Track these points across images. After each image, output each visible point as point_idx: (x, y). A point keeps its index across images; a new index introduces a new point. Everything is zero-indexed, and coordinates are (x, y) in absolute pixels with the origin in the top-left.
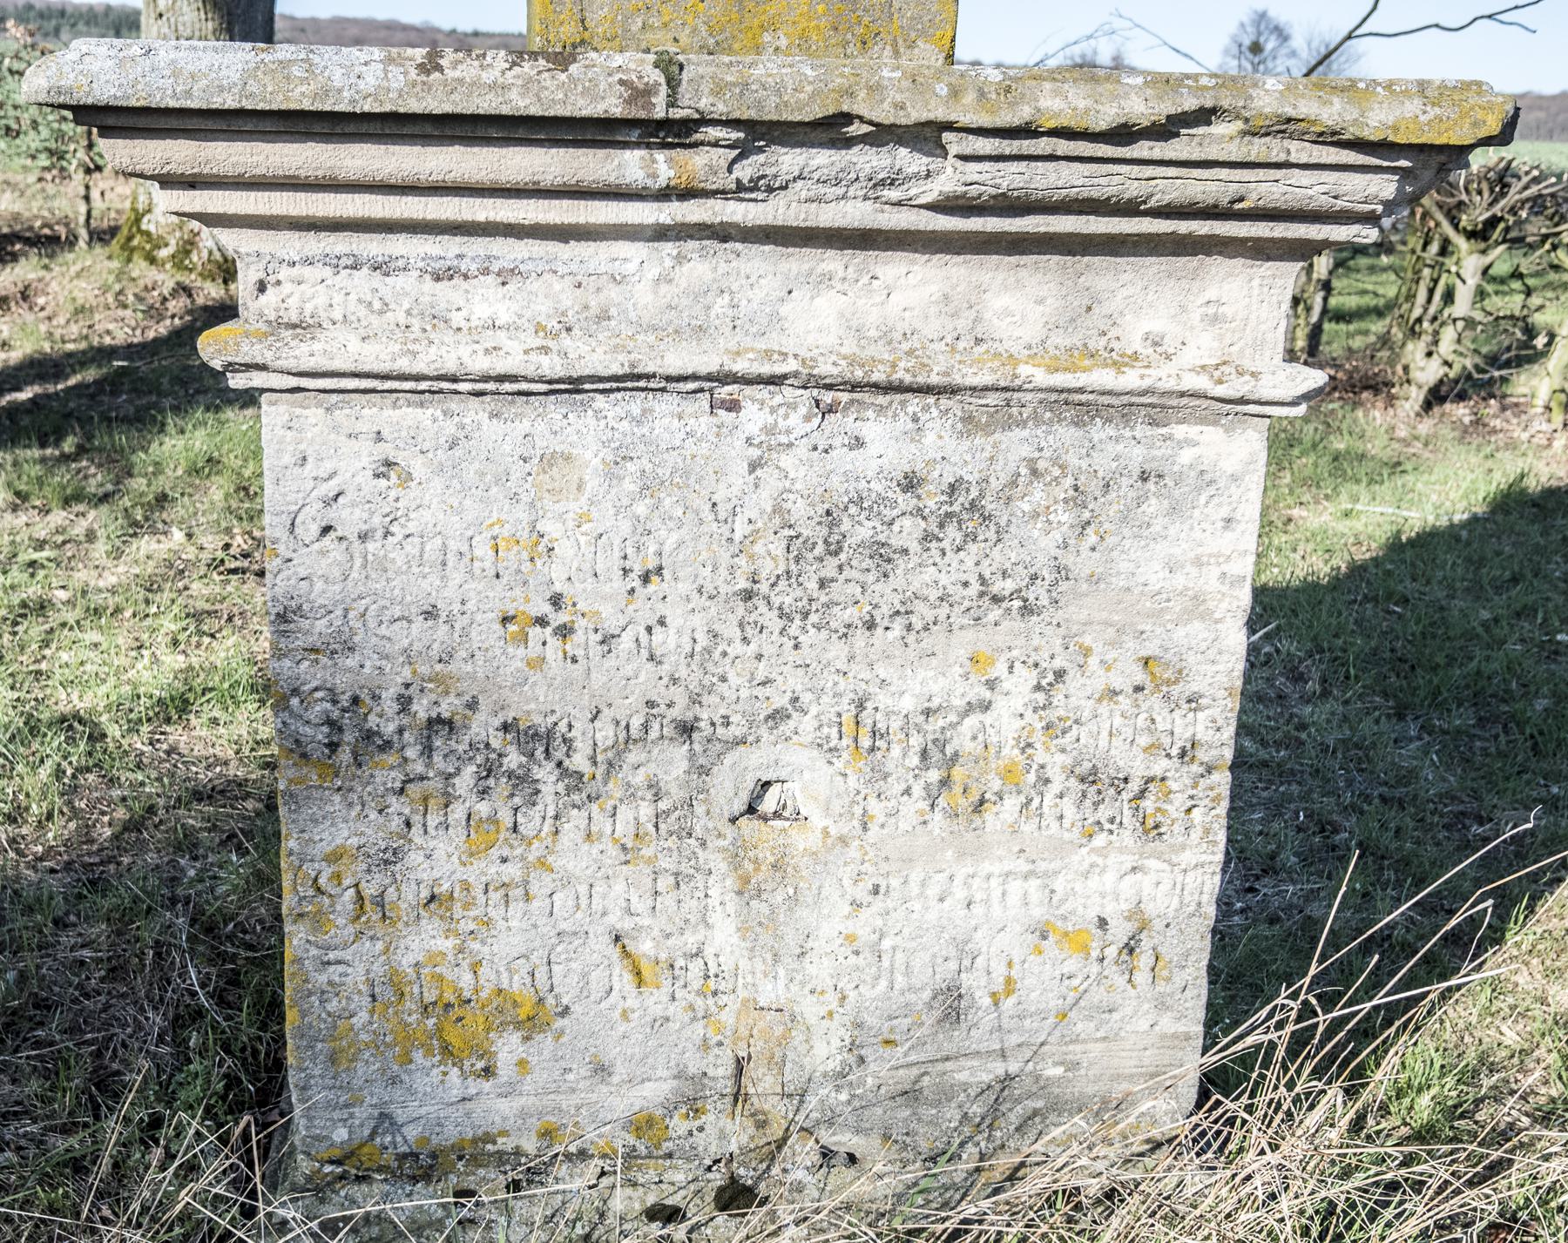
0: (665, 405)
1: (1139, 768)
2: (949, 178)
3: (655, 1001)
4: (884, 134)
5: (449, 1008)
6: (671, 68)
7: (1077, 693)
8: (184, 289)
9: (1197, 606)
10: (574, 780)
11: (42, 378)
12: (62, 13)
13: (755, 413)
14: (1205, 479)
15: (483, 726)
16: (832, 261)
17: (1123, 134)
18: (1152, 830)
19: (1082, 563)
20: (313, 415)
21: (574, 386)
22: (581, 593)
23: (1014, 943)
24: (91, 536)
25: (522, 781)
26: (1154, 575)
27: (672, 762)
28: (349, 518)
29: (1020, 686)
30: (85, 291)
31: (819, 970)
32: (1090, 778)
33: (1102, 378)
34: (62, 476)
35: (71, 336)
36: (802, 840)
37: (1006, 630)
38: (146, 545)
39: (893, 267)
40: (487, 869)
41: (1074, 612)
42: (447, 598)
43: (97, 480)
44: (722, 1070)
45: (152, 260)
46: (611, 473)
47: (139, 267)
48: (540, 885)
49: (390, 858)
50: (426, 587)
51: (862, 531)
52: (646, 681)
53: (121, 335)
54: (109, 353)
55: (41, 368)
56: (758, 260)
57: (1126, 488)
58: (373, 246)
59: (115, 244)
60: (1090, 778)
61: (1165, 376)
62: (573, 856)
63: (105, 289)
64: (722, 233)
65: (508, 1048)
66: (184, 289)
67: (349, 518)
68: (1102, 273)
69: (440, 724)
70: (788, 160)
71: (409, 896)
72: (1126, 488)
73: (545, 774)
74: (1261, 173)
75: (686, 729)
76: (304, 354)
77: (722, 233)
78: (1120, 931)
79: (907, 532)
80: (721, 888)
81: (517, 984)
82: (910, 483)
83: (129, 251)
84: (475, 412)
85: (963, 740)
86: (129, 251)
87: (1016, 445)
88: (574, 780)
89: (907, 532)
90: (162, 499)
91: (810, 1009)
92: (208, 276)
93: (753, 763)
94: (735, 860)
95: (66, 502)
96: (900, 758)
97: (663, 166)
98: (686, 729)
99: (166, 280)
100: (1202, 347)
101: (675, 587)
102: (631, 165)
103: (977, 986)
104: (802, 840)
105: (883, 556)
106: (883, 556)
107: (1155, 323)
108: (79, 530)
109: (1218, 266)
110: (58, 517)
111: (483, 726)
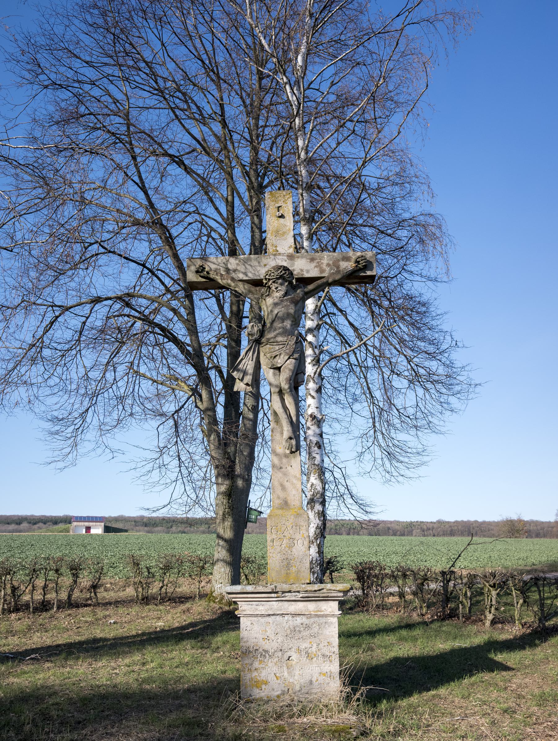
0: (278, 617)
1: (329, 654)
2: (301, 595)
3: (279, 681)
4: (294, 592)
5: (257, 682)
6: (276, 587)
7: (321, 646)
8: (221, 608)
9: (333, 636)
10: (270, 656)
11: (193, 627)
12: (174, 521)
13: (286, 617)
14: (332, 623)
15: (261, 650)
16: (293, 603)
17: (315, 591)
18: (331, 661)
19: (320, 632)
20: (245, 619)
21: (269, 615)
22: (270, 636)
23: (317, 675)
24: (206, 653)
25: (265, 656)
26: (328, 633)
27: (280, 654)
28: (248, 629)
29: (315, 645)
30: (200, 609)
31: (296, 678)
32: (323, 655)
33: (319, 613)
34: (199, 644)
35: (197, 618)
36: (294, 663)
37: (313, 639)
38: (216, 654)
39: (299, 603)
40: (261, 666)
41: (320, 637)
42: (257, 637)
43: (205, 645)
44: (286, 690)
45: (214, 602)
46: (273, 624)
47: (212, 604)
48: (267, 667)
49: (252, 664)
50: (255, 635)
51: (298, 629)
52: (277, 645)
53: (207, 618)
54: (205, 622)
55: (192, 625)
56: (286, 603)
57: (324, 624)
58: (251, 603)
59: (207, 599)
60: (323, 655)
61: (326, 613)
62: (270, 664)
63: (205, 608)
64: (282, 601)
65: (263, 687)
66: (221, 608)
67: (248, 629)
68: (319, 603)
69: (256, 650)
70: (287, 594)
71: (253, 669)
72: (324, 624)
73: (267, 655)
74: (291, 599)
75: (281, 650)
76: (245, 613)
77: (282, 601)
78: (329, 673)
79: (302, 629)
80: (285, 668)
81: (264, 679)
82: (302, 624)
83: (210, 600)
84: (260, 618)
85: (310, 651)
86: (210, 600)
87: (312, 620)
88: (270, 656)
89: (302, 629)
90: (218, 648)
91: (296, 683)
92: (226, 605)
93: (288, 654)
94: (287, 665)
95: (201, 648)
96: (303, 653)
97: (276, 595)
98: (281, 650)
99: (217, 606)
100: (330, 610)
101: (279, 635)
102: (273, 595)
103: (314, 680)
104: (294, 663)
105: (300, 632)
106: (300, 632)
107: (325, 608)
108: (204, 652)
109: (330, 602)
110: (200, 651)
111: (261, 650)
